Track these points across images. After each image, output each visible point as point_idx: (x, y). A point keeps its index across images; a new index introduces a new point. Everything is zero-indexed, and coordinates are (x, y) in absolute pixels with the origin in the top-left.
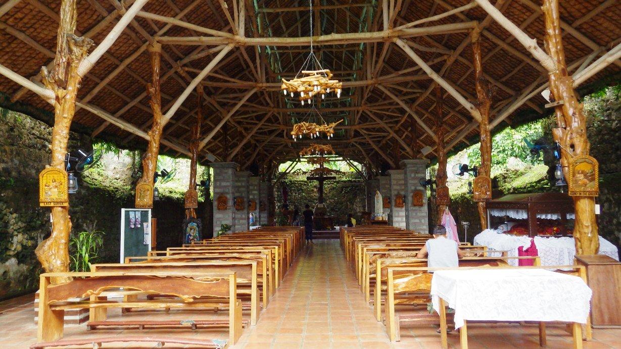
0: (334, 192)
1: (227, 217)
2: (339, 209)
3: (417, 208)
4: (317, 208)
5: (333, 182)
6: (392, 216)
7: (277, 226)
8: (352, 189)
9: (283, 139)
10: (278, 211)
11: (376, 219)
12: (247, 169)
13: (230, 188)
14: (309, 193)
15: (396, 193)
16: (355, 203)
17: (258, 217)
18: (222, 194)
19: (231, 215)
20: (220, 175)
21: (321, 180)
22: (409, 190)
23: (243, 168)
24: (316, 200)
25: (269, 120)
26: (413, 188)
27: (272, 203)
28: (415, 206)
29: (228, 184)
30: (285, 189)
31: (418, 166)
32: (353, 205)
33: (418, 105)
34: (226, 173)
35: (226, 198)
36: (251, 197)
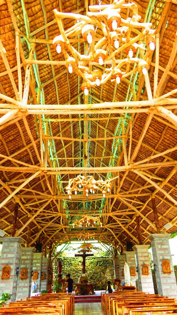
0: (92, 265)
1: (8, 286)
2: (96, 278)
3: (166, 275)
4: (82, 277)
5: (91, 258)
6: (140, 283)
7: (54, 293)
8: (104, 263)
9: (59, 225)
10: (55, 279)
11: (126, 285)
12: (32, 246)
13: (14, 260)
14: (76, 266)
15: (142, 263)
16: (106, 273)
17: (39, 285)
18: (7, 264)
19: (12, 284)
20: (7, 248)
21: (84, 256)
22: (158, 259)
23: (30, 244)
24: (81, 271)
25: (48, 208)
26: (161, 258)
27: (50, 273)
28: (164, 273)
29: (13, 256)
30: (60, 263)
31: (163, 239)
32: (105, 274)
33: (156, 194)
34: (12, 246)
35: (10, 268)
36: (34, 268)
